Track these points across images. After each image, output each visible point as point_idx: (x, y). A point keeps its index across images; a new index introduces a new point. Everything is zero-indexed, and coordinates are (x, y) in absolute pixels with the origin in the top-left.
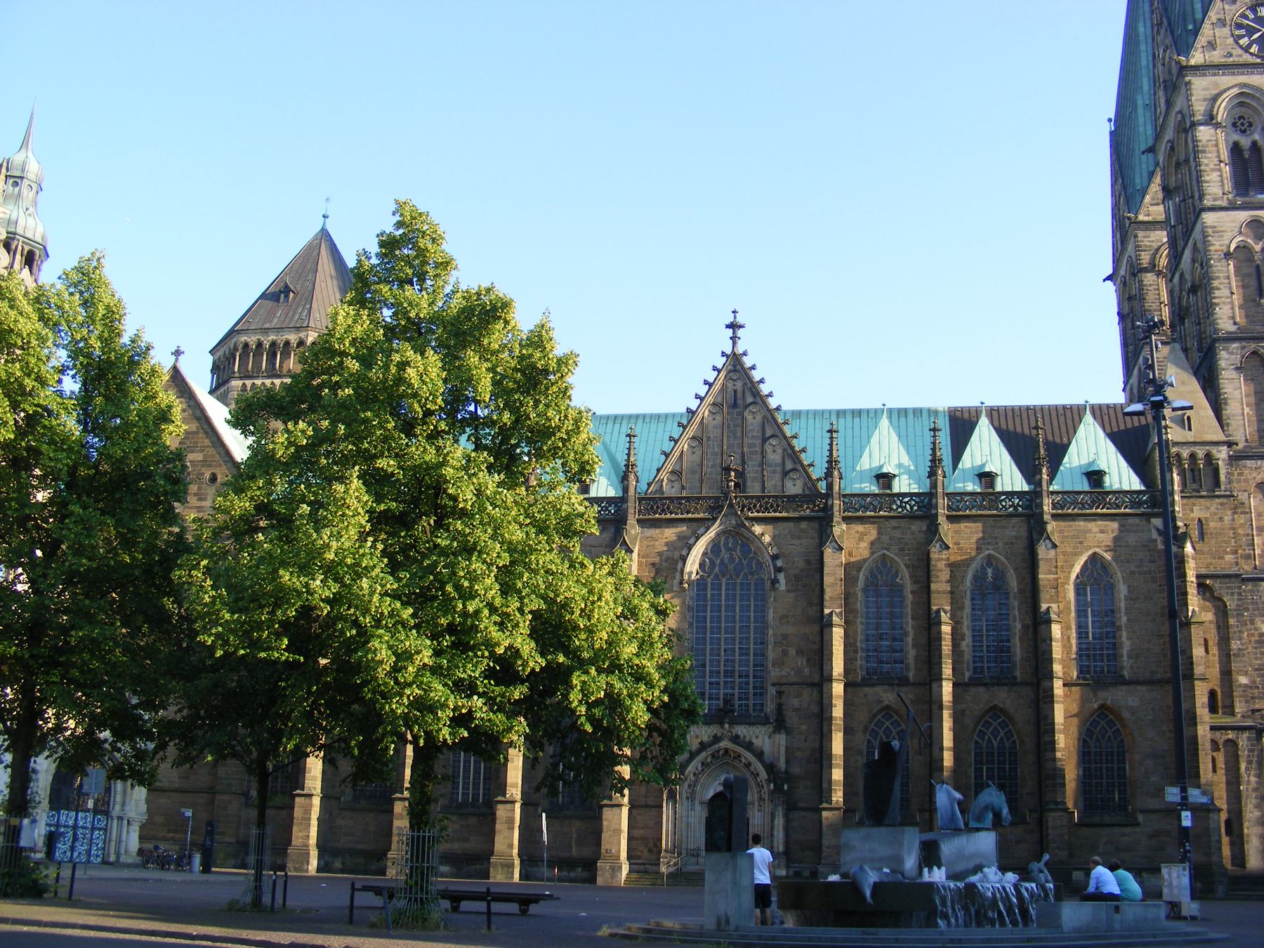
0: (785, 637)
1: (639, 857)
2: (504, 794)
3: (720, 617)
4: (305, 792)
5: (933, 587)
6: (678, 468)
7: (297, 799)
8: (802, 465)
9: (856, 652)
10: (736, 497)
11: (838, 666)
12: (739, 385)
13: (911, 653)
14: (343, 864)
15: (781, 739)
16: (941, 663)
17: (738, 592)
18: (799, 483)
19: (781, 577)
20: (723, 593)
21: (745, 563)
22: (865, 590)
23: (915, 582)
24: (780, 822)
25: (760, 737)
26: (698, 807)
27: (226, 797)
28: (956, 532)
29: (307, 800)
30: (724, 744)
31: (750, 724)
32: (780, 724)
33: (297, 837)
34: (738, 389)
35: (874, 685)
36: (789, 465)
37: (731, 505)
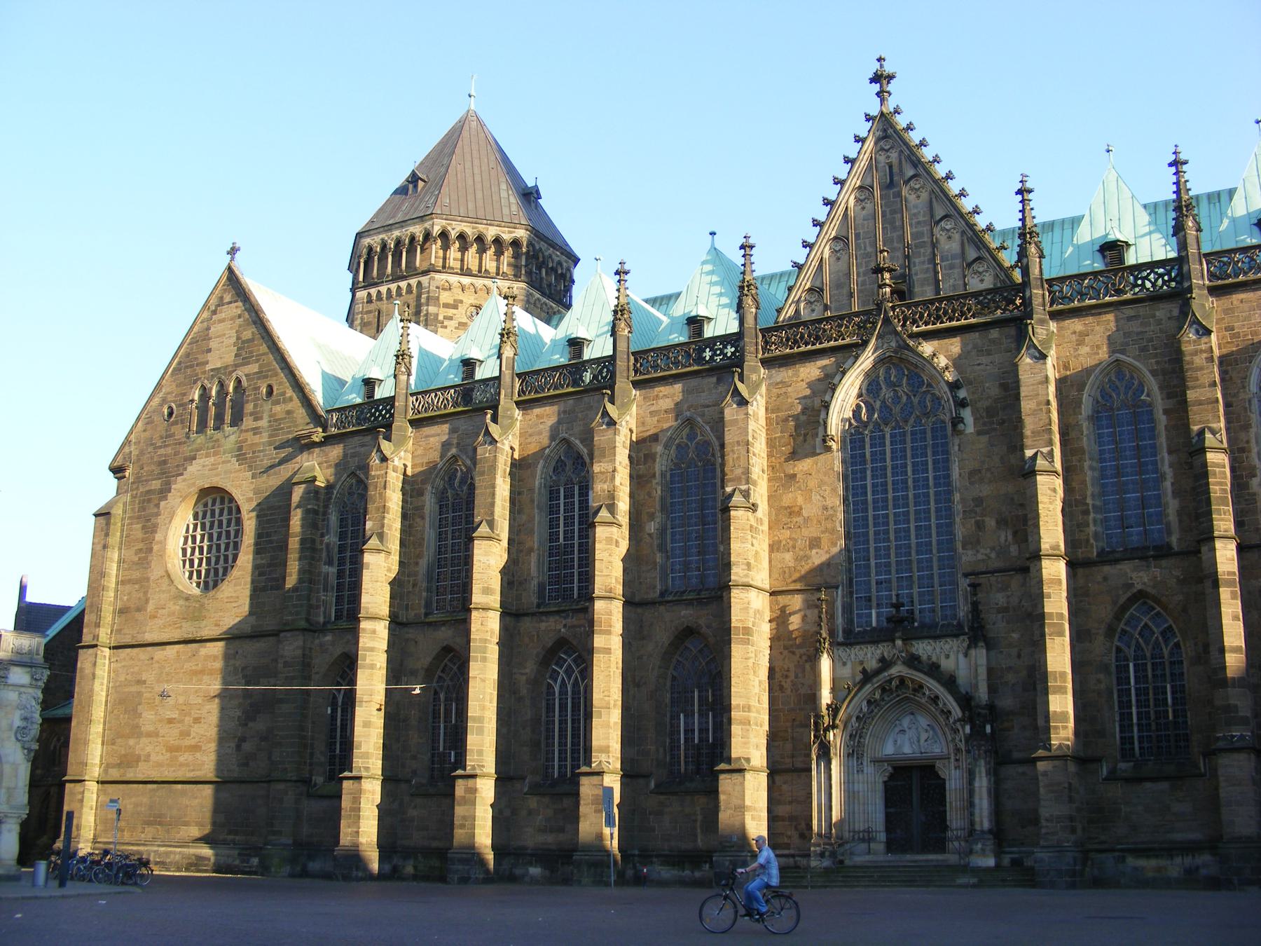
0: (979, 501)
1: (787, 846)
2: (589, 764)
3: (885, 484)
4: (354, 773)
5: (1191, 395)
6: (818, 284)
7: (346, 784)
8: (988, 250)
9: (1086, 512)
10: (893, 308)
11: (1052, 532)
12: (894, 155)
14: (415, 867)
15: (980, 655)
16: (1210, 513)
17: (909, 445)
19: (967, 414)
20: (888, 449)
21: (915, 400)
22: (1095, 418)
24: (982, 783)
25: (953, 656)
26: (869, 769)
27: (281, 786)
28: (1226, 311)
29: (356, 785)
30: (897, 670)
33: (346, 834)
34: (896, 165)
35: (1116, 561)
36: (972, 254)
37: (887, 321)
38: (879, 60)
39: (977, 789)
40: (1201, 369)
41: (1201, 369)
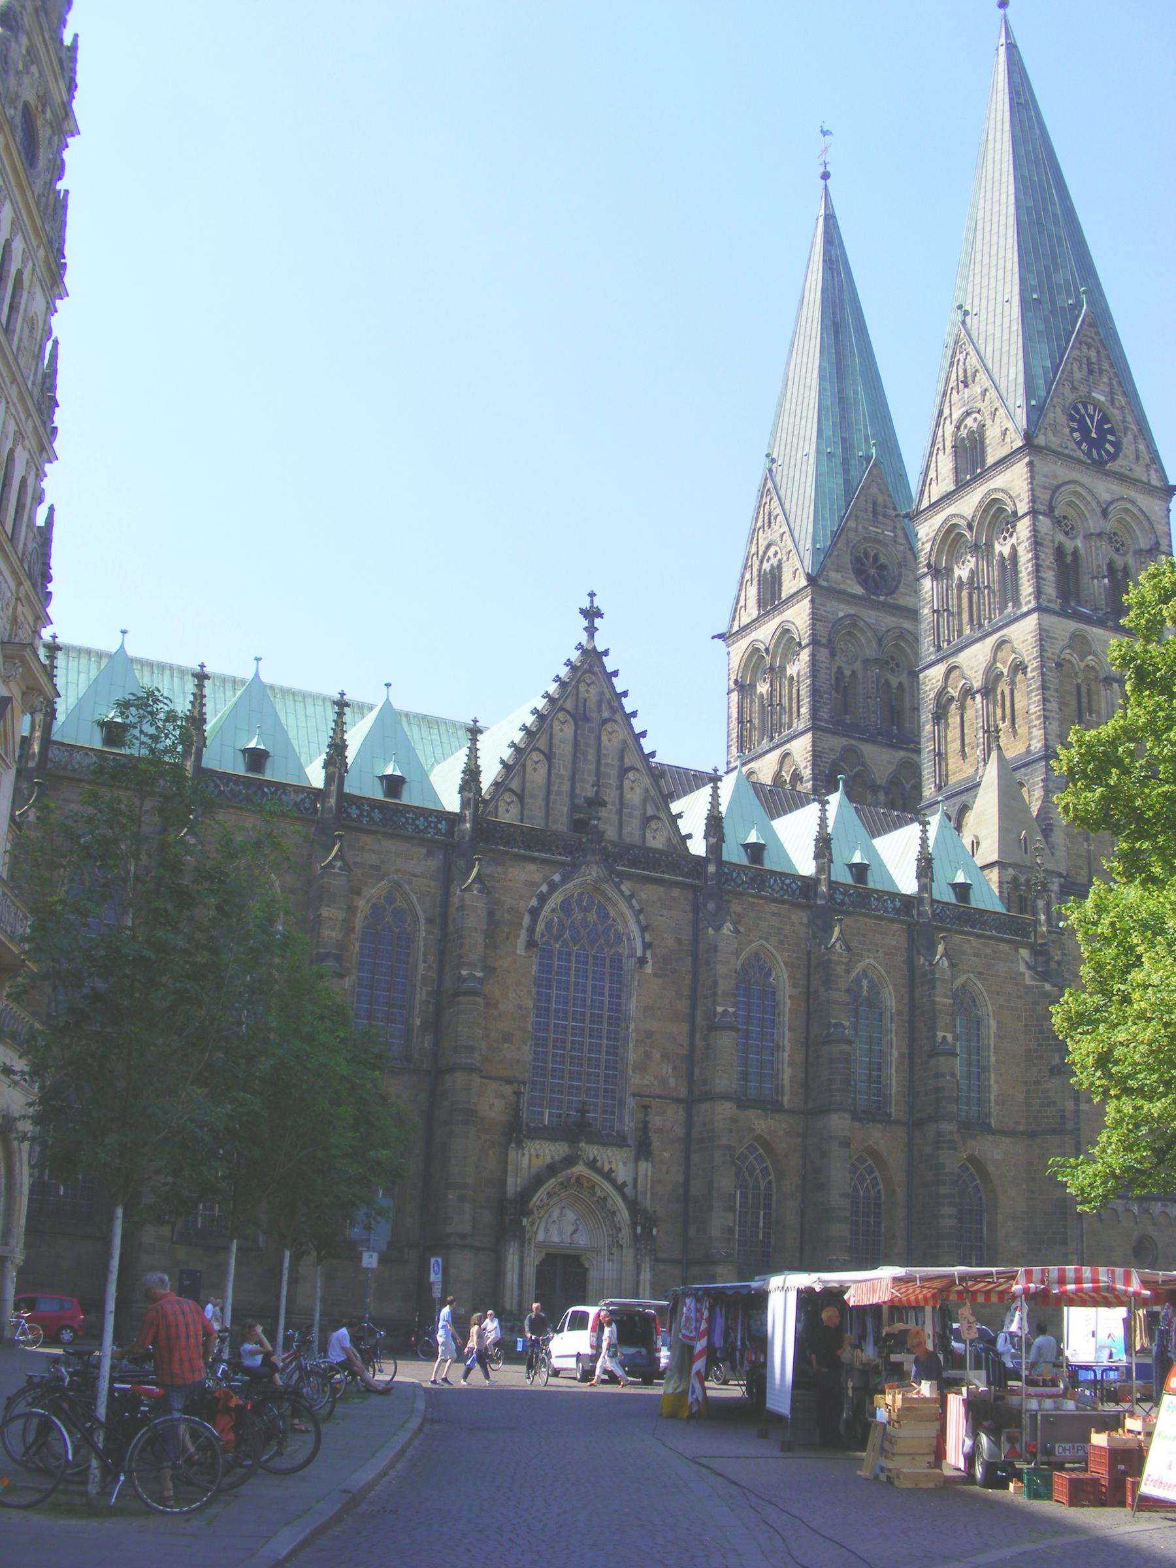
0: (649, 1034)
13: (787, 1073)
23: (794, 986)
25: (619, 1162)
30: (580, 1169)
31: (604, 1145)
32: (643, 1150)
38: (124, 632)
39: (642, 1282)
40: (841, 976)
41: (841, 976)
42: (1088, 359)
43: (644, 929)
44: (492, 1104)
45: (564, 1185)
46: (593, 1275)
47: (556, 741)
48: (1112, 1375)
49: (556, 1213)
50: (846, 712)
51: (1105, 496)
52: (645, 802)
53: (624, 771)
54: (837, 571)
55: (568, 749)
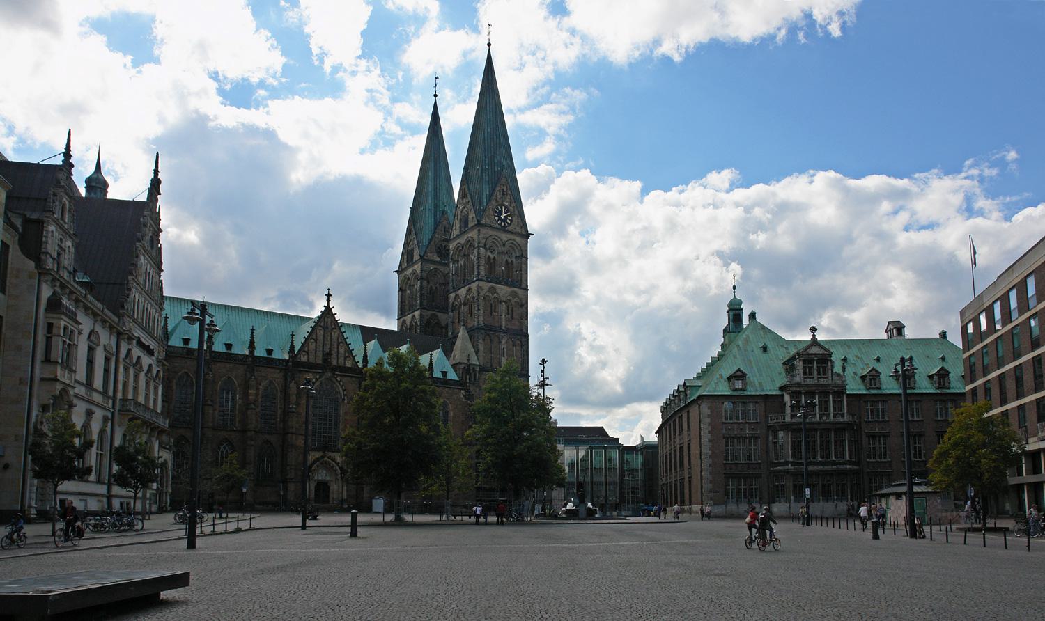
0: (346, 420)
18: (350, 362)
30: (326, 459)
36: (347, 355)
42: (503, 190)
43: (344, 390)
44: (300, 442)
45: (322, 464)
46: (331, 488)
47: (318, 336)
48: (377, 497)
49: (320, 471)
50: (433, 301)
51: (505, 239)
52: (345, 352)
53: (339, 343)
54: (431, 253)
55: (322, 337)
